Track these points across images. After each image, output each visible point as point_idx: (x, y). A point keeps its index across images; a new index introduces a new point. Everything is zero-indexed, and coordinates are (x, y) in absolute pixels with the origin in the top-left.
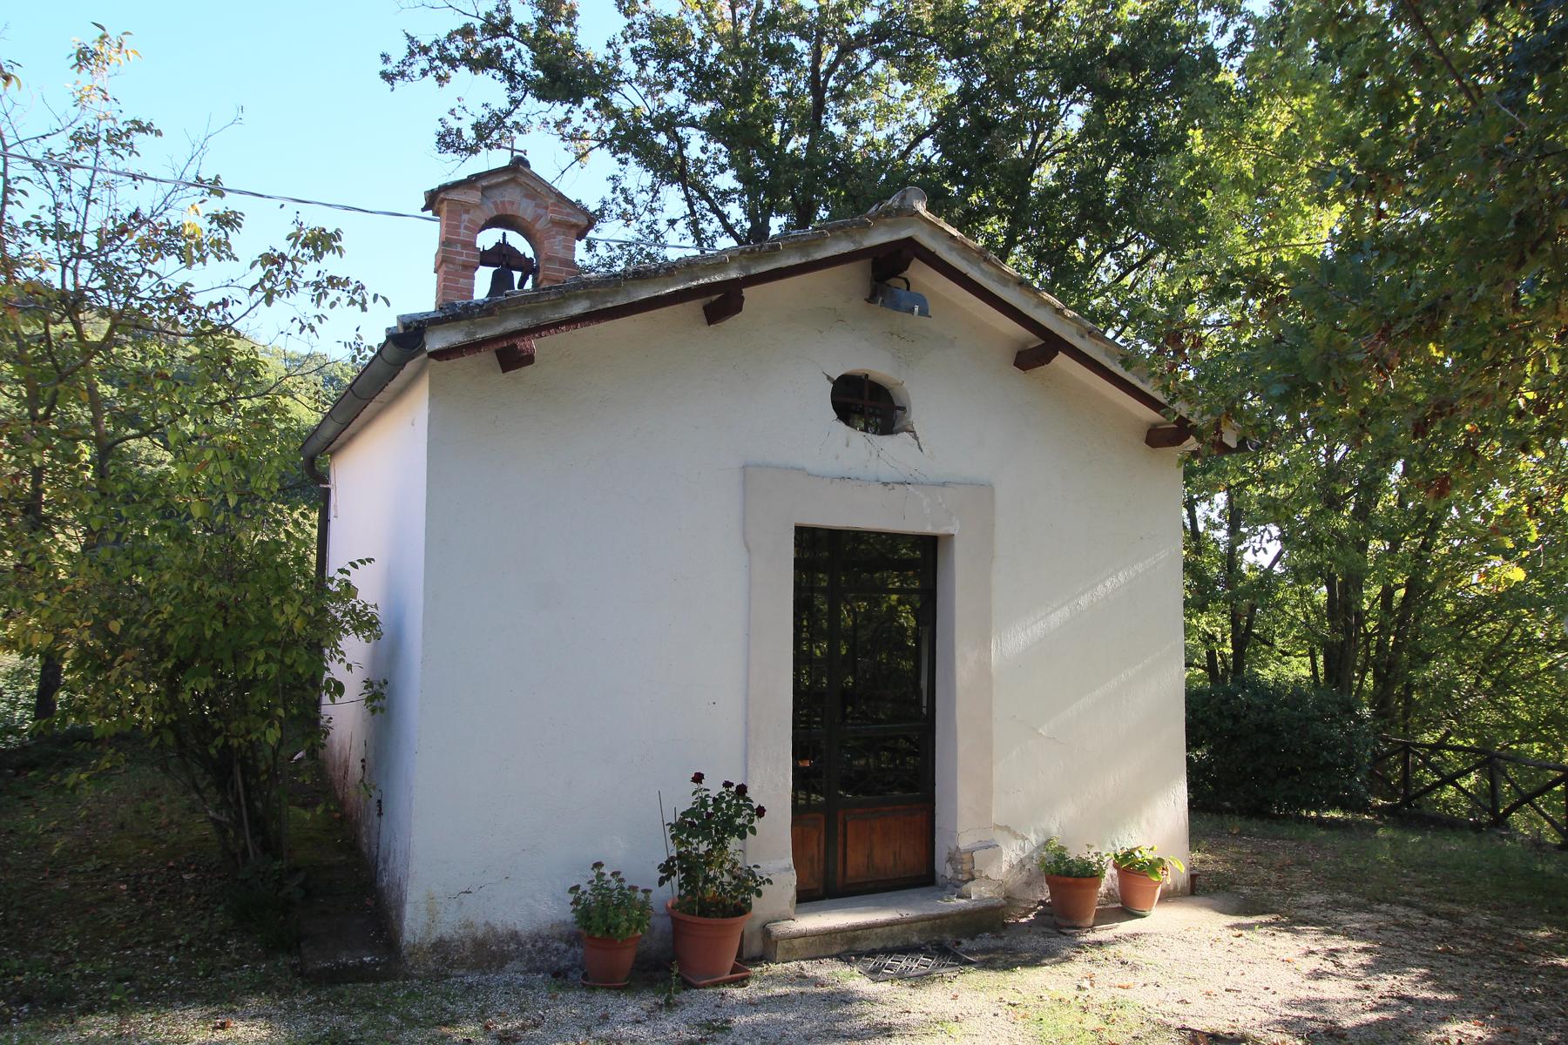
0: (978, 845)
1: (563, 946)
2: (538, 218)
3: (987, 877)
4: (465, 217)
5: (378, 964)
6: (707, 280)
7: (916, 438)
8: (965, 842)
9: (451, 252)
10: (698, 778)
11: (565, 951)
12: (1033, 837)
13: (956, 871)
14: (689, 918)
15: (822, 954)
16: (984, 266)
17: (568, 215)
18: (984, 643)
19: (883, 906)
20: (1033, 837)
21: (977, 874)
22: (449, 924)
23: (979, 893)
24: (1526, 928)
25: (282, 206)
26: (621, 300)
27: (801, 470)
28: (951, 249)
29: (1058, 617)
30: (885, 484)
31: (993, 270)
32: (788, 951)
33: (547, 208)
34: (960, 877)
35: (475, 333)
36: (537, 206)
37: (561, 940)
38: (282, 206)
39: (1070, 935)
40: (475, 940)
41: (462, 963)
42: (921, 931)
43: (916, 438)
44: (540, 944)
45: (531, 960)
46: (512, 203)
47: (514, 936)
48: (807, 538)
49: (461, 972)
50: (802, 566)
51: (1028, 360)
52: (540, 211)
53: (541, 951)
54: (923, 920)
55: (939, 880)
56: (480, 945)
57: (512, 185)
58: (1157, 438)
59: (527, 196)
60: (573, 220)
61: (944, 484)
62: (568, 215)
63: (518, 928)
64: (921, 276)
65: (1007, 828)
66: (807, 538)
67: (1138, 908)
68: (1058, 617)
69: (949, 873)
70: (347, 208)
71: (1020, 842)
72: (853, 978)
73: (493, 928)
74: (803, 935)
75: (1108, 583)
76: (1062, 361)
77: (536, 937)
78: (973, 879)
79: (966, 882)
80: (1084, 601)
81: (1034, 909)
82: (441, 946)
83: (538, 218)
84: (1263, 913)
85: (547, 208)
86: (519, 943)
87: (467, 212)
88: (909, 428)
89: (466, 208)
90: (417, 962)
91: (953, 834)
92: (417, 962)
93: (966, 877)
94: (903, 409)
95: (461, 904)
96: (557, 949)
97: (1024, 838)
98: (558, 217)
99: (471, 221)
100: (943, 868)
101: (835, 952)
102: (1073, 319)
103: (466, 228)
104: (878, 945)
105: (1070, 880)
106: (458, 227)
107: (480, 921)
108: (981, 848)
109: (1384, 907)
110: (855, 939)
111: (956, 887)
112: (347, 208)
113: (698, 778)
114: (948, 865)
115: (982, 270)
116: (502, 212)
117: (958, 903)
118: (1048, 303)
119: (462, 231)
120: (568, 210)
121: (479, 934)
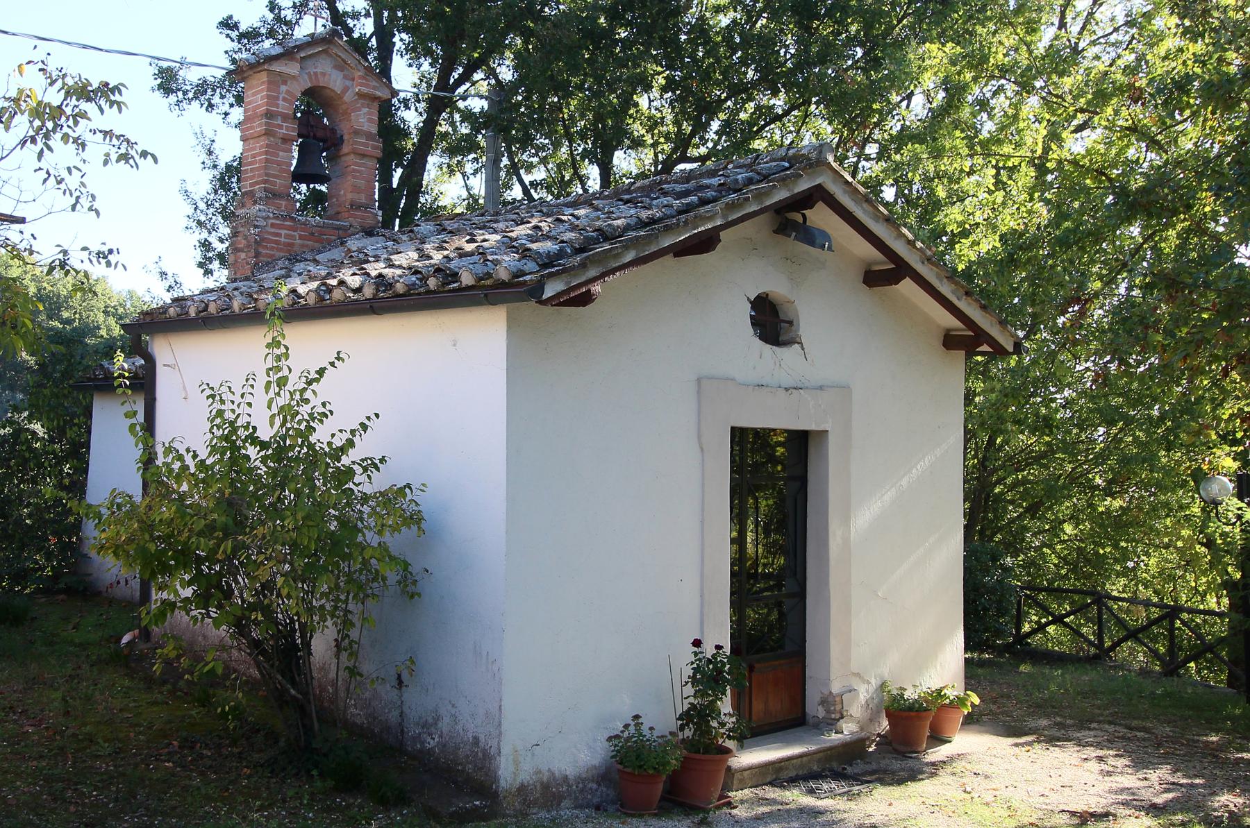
0: (844, 689)
1: (595, 786)
2: (346, 89)
3: (851, 716)
4: (283, 88)
5: (485, 806)
6: (703, 228)
7: (803, 349)
8: (836, 688)
9: (274, 126)
10: (697, 643)
11: (596, 790)
12: (873, 681)
13: (828, 712)
14: (697, 756)
15: (760, 782)
16: (865, 205)
17: (374, 88)
18: (846, 520)
19: (788, 743)
20: (873, 681)
21: (845, 713)
22: (525, 775)
23: (849, 729)
24: (1199, 735)
25: (35, 47)
26: (654, 248)
27: (733, 380)
28: (845, 192)
29: (889, 496)
30: (787, 389)
31: (871, 209)
32: (741, 781)
33: (353, 80)
34: (833, 716)
35: (570, 282)
36: (345, 77)
37: (593, 781)
38: (35, 47)
39: (915, 758)
40: (542, 783)
41: (535, 803)
42: (819, 761)
43: (803, 349)
44: (581, 785)
45: (576, 798)
46: (324, 74)
47: (566, 778)
48: (739, 436)
49: (535, 811)
50: (737, 466)
51: (873, 278)
52: (348, 83)
53: (582, 791)
54: (821, 752)
55: (810, 720)
56: (545, 787)
57: (324, 56)
58: (950, 341)
59: (337, 67)
60: (378, 93)
61: (821, 388)
62: (374, 88)
63: (568, 773)
64: (820, 216)
65: (858, 675)
66: (739, 436)
67: (946, 736)
68: (889, 496)
69: (821, 713)
70: (85, 47)
71: (866, 686)
72: (797, 797)
73: (553, 774)
74: (750, 768)
75: (919, 467)
76: (907, 286)
77: (579, 780)
78: (842, 717)
79: (838, 720)
80: (904, 482)
81: (874, 741)
82: (522, 789)
83: (346, 89)
84: (1026, 734)
85: (353, 80)
86: (569, 786)
87: (285, 83)
88: (798, 340)
89: (284, 78)
90: (509, 804)
91: (827, 681)
92: (509, 804)
93: (838, 716)
94: (790, 323)
95: (533, 755)
96: (591, 789)
97: (869, 683)
98: (365, 90)
99: (288, 92)
100: (814, 708)
101: (768, 780)
102: (920, 250)
103: (284, 99)
104: (793, 774)
105: (912, 714)
106: (277, 98)
107: (544, 768)
108: (846, 692)
109: (1094, 725)
110: (781, 769)
111: (831, 723)
112: (85, 47)
113: (697, 643)
114: (820, 708)
115: (864, 209)
116: (315, 84)
117: (835, 738)
118: (904, 236)
119: (281, 102)
120: (374, 83)
121: (545, 779)
